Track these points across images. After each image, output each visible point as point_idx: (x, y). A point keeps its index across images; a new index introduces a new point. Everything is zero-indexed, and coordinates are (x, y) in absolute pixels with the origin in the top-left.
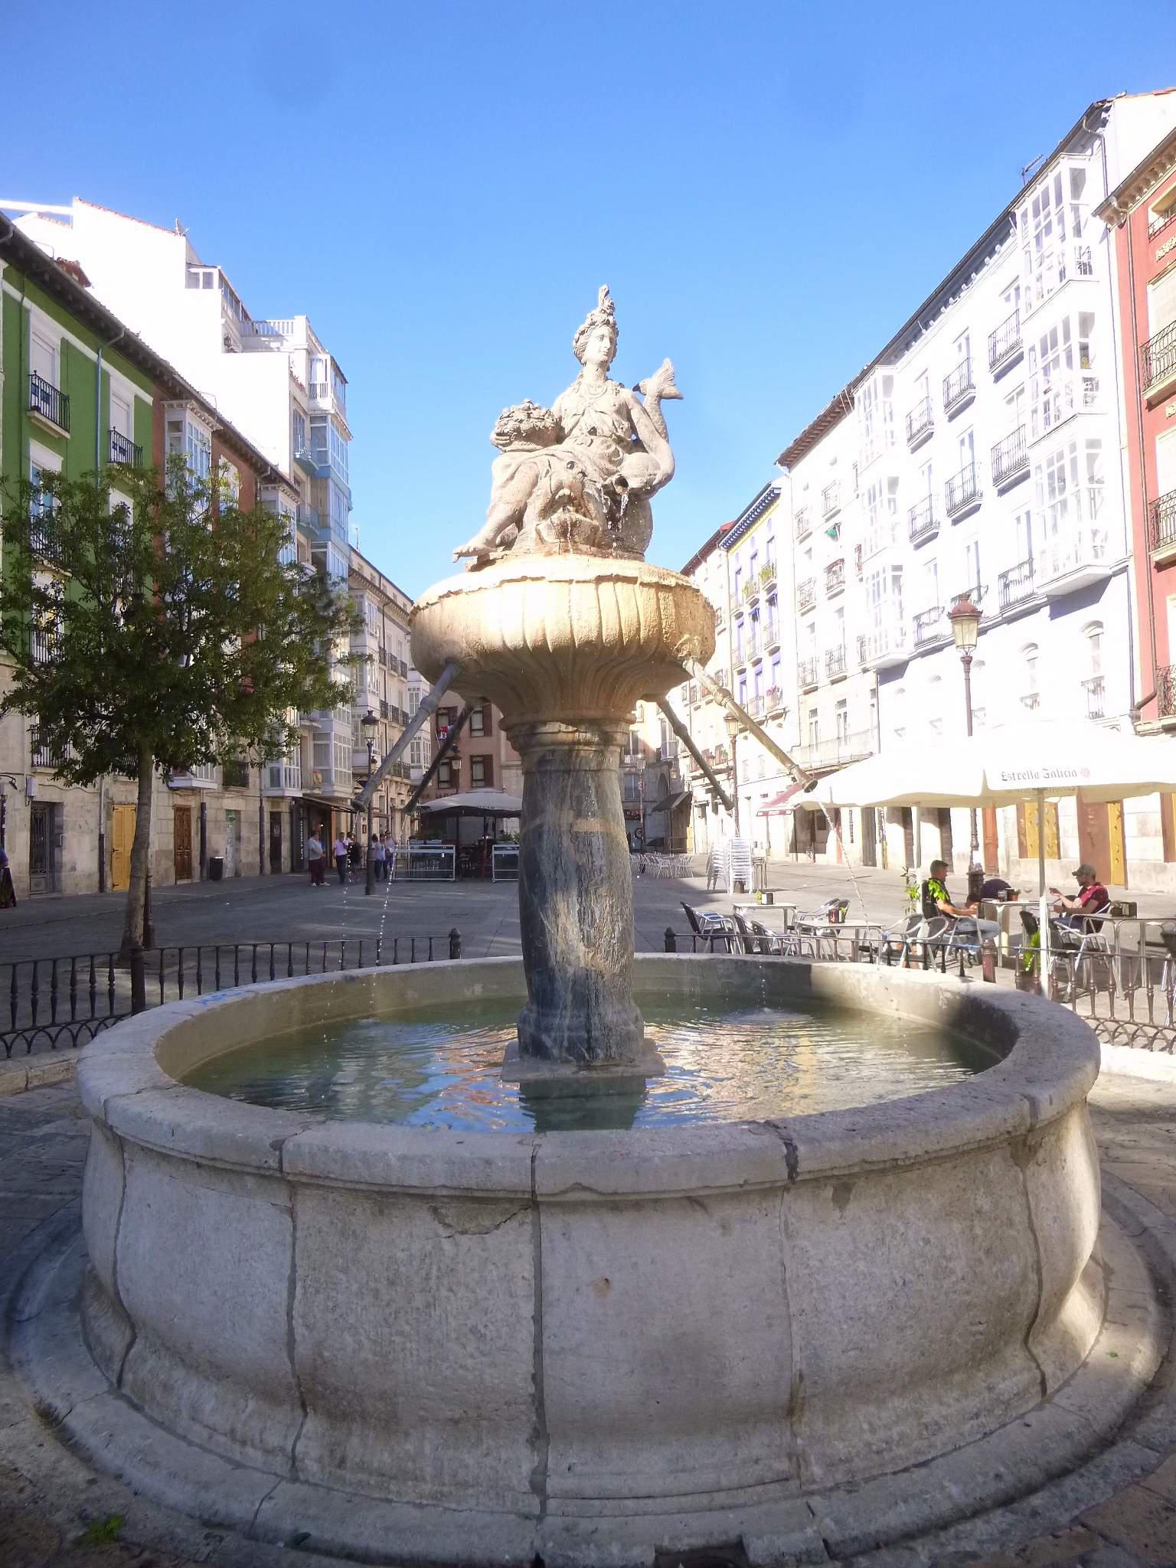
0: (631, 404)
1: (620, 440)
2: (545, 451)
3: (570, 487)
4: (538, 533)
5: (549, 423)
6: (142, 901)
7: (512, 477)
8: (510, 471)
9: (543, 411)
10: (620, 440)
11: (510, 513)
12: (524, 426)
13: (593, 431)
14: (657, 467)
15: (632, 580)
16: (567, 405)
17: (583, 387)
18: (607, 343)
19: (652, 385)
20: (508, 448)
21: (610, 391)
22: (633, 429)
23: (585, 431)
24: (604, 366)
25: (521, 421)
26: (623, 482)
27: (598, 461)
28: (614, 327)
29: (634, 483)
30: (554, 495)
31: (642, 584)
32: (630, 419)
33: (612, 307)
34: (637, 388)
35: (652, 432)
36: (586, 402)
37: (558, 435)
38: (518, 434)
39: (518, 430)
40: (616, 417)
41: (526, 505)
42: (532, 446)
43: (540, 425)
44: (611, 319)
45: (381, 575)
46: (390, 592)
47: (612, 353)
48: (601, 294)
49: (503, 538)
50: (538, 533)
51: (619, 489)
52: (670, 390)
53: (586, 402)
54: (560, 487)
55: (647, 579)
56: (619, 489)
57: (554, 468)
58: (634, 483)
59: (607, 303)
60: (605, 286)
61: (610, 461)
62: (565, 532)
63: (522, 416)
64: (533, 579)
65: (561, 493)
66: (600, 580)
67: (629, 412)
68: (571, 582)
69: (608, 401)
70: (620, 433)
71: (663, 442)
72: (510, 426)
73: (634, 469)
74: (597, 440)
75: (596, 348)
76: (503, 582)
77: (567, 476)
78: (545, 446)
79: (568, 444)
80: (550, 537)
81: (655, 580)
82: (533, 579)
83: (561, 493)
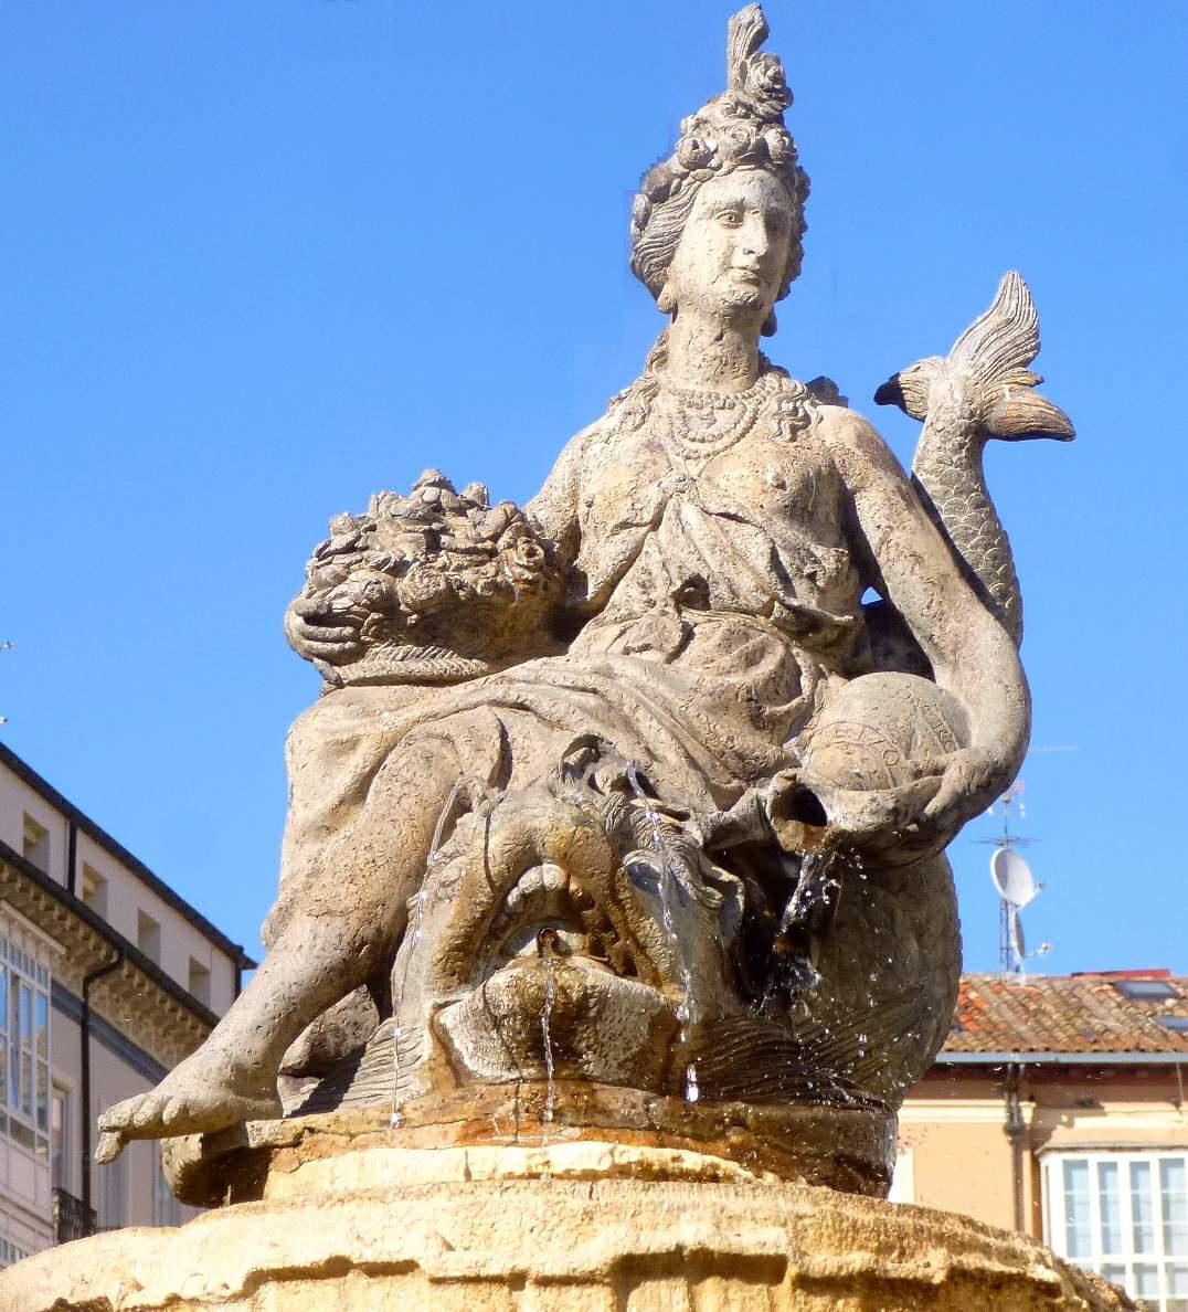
0: (858, 469)
1: (803, 626)
2: (492, 686)
3: (565, 860)
4: (443, 1040)
5: (515, 565)
6: (889, 775)
7: (360, 791)
8: (357, 762)
9: (495, 517)
10: (803, 626)
11: (334, 956)
12: (411, 588)
13: (694, 593)
14: (954, 733)
15: (763, 1269)
16: (596, 474)
17: (666, 404)
18: (753, 235)
19: (946, 384)
20: (350, 672)
21: (767, 424)
22: (863, 565)
23: (661, 592)
24: (749, 323)
25: (399, 569)
26: (803, 805)
27: (704, 723)
28: (789, 177)
29: (847, 812)
30: (501, 887)
31: (806, 1283)
32: (850, 534)
33: (779, 91)
34: (890, 394)
35: (941, 584)
36: (669, 471)
37: (556, 607)
38: (386, 618)
39: (386, 604)
40: (783, 529)
41: (402, 920)
42: (447, 662)
43: (474, 579)
44: (772, 137)
45: (77, 821)
46: (123, 908)
47: (778, 270)
48: (738, 46)
49: (316, 1046)
50: (443, 1040)
51: (789, 834)
52: (1017, 402)
53: (669, 471)
54: (526, 857)
55: (823, 1261)
56: (789, 834)
57: (516, 758)
58: (847, 812)
59: (758, 77)
60: (747, 14)
61: (757, 721)
62: (553, 1038)
63: (402, 543)
64: (377, 1270)
65: (529, 881)
66: (630, 1271)
67: (846, 505)
68: (516, 1280)
69: (751, 471)
70: (805, 598)
71: (984, 630)
72: (360, 584)
73: (852, 741)
74: (710, 630)
75: (713, 251)
76: (257, 1279)
77: (543, 809)
78: (501, 658)
79: (593, 645)
80: (484, 1061)
81: (857, 1260)
82: (377, 1270)
83: (529, 881)
